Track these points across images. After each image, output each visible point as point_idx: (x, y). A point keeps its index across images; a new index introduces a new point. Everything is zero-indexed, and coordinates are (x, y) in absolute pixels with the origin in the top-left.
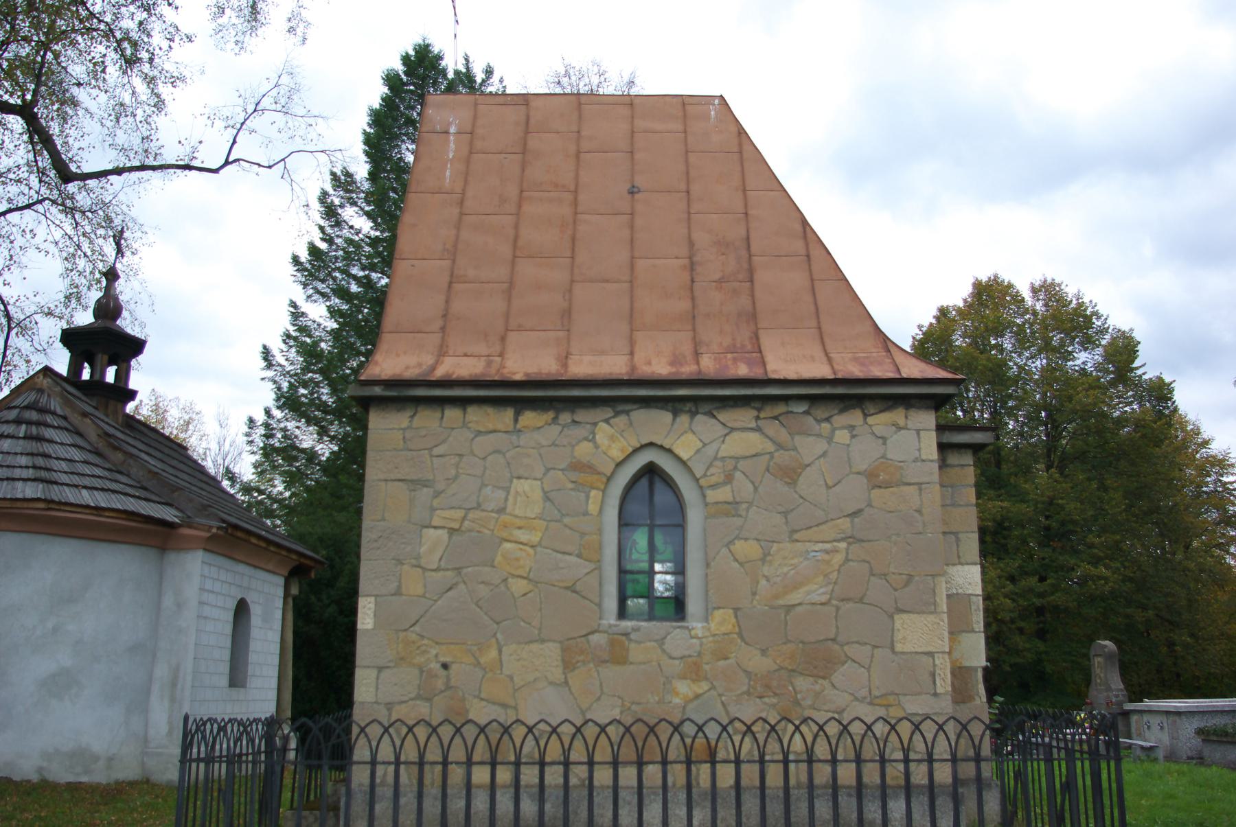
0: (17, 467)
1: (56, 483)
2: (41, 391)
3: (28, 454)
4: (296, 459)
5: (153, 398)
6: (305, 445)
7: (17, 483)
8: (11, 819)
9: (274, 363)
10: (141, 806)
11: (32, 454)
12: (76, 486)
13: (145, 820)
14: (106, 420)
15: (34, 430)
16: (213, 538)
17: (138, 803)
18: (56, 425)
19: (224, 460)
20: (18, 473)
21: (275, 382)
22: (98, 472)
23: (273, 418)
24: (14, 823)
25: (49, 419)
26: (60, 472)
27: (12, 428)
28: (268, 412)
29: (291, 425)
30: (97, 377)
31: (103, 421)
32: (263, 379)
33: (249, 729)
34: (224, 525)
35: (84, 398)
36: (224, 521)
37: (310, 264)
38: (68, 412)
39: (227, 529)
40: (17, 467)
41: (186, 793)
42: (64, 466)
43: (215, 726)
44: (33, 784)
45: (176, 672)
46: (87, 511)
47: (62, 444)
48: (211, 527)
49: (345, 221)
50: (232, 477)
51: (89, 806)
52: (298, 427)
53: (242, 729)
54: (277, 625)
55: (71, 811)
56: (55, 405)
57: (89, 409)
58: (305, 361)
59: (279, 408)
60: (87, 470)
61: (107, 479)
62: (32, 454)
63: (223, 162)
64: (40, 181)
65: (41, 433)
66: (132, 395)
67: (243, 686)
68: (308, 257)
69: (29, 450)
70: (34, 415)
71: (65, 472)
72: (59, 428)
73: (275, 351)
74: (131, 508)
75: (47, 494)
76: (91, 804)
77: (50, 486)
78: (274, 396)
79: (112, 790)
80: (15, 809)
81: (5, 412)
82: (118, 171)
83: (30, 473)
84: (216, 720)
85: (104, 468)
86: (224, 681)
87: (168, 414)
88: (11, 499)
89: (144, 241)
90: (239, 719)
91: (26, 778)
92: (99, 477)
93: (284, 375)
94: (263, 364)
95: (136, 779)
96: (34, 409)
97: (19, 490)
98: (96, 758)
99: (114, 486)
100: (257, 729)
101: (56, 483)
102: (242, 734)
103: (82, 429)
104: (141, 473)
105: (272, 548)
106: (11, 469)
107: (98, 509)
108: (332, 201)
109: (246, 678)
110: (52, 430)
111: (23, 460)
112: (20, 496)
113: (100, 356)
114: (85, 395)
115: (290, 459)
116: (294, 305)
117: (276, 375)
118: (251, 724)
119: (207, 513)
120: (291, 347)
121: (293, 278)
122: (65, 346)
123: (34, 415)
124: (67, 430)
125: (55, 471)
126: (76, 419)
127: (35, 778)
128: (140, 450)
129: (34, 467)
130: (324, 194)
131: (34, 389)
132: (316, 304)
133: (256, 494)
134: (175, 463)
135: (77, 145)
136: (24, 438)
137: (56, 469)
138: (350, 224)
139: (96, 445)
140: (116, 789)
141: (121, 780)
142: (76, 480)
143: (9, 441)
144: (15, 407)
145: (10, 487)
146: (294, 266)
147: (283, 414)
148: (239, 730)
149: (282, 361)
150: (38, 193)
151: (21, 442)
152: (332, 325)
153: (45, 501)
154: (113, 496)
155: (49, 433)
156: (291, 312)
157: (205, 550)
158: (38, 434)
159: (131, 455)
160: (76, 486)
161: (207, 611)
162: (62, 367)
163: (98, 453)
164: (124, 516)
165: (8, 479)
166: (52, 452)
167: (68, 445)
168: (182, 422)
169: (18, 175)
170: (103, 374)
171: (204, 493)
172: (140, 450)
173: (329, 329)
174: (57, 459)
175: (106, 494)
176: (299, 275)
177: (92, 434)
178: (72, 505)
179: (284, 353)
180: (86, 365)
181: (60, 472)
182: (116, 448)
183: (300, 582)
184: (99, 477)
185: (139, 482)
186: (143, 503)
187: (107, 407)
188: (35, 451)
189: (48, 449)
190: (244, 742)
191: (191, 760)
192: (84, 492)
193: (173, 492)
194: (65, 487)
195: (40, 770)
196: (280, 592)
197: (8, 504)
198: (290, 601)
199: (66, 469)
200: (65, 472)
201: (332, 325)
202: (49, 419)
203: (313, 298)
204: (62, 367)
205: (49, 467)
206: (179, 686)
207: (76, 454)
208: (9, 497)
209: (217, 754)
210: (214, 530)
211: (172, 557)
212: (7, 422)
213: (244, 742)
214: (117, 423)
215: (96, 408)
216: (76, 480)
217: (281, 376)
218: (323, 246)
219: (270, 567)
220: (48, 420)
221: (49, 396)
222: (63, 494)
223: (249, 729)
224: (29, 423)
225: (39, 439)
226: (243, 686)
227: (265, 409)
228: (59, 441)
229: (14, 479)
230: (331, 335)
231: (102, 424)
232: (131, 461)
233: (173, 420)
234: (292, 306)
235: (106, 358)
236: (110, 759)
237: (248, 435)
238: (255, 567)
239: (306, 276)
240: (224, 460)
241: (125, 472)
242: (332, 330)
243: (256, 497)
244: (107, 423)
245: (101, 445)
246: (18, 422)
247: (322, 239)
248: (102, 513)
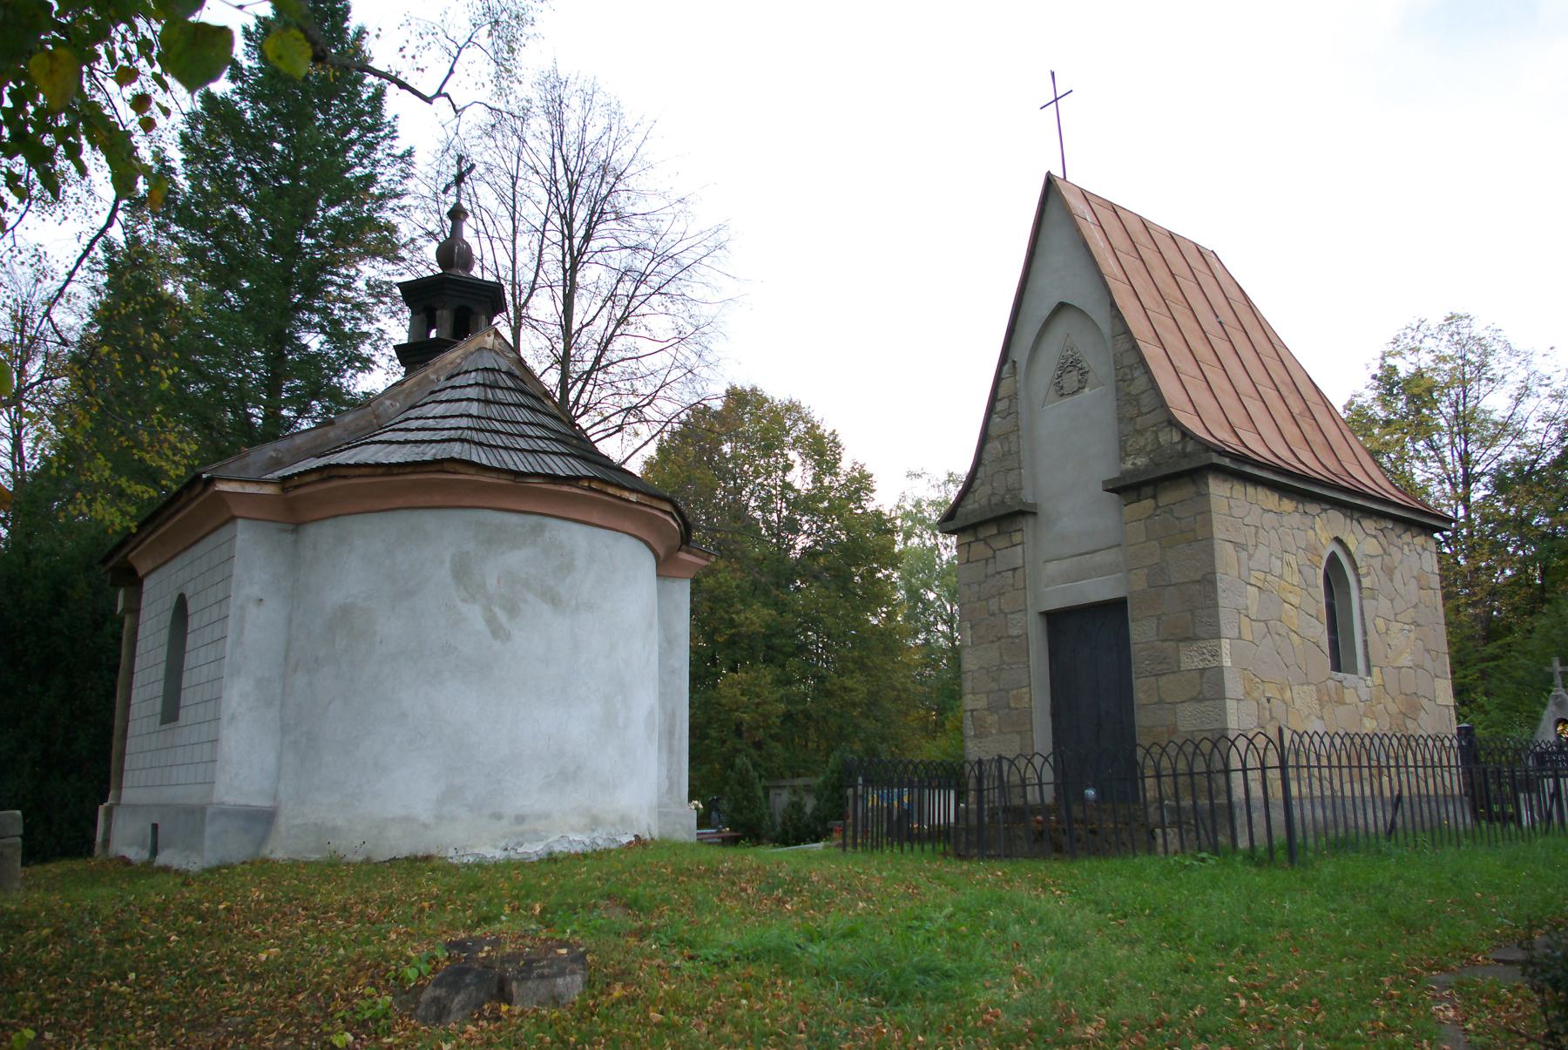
206: (677, 736)
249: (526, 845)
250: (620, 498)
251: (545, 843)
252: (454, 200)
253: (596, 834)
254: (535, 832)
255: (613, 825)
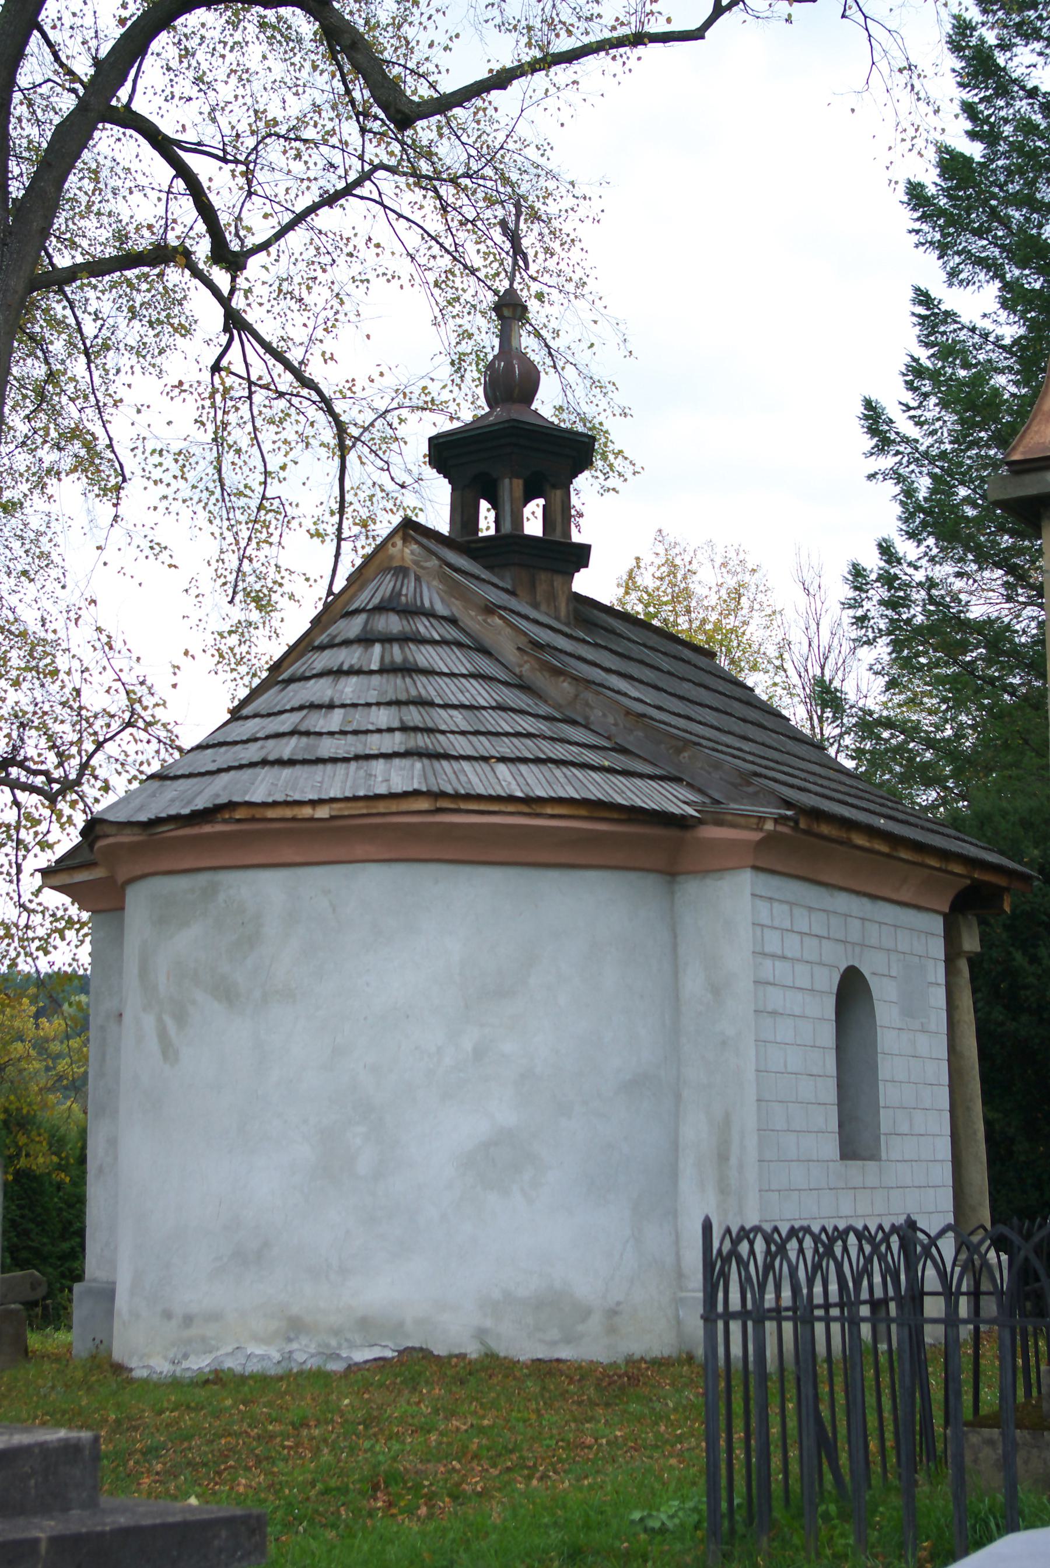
0: (372, 732)
1: (447, 757)
2: (402, 571)
3: (389, 704)
4: (964, 647)
5: (661, 549)
6: (976, 612)
7: (374, 763)
8: (429, 1432)
9: (893, 436)
10: (675, 1410)
11: (398, 703)
12: (485, 759)
13: (680, 1439)
14: (533, 614)
15: (397, 653)
16: (769, 842)
17: (671, 1404)
18: (437, 637)
19: (822, 668)
20: (328, 747)
21: (900, 479)
22: (527, 724)
23: (899, 561)
24: (433, 1437)
25: (423, 627)
26: (453, 732)
27: (357, 655)
28: (886, 550)
29: (944, 571)
30: (507, 528)
31: (526, 618)
32: (872, 476)
33: (883, 1248)
34: (789, 813)
35: (485, 575)
36: (788, 804)
37: (950, 197)
38: (457, 608)
39: (797, 822)
40: (372, 732)
41: (722, 1384)
42: (459, 719)
43: (808, 1242)
44: (470, 1362)
45: (724, 1128)
46: (510, 808)
47: (452, 675)
48: (762, 819)
49: (1014, 81)
50: (832, 700)
51: (574, 1407)
52: (959, 575)
53: (868, 1249)
54: (939, 1021)
55: (540, 1415)
56: (432, 597)
57: (495, 596)
58: (962, 421)
59: (911, 535)
60: (504, 723)
61: (545, 738)
62: (398, 703)
63: (708, 10)
64: (363, 131)
65: (411, 659)
66: (580, 556)
67: (873, 1155)
68: (938, 181)
69: (390, 696)
70: (392, 624)
71: (463, 733)
72: (444, 642)
73: (893, 412)
74: (595, 793)
75: (432, 780)
76: (579, 1403)
77: (436, 764)
78: (898, 510)
79: (620, 1377)
80: (436, 1411)
81: (342, 624)
82: (501, 80)
83: (396, 742)
84: (807, 1230)
85: (536, 716)
86: (831, 1147)
87: (695, 578)
88: (366, 798)
89: (582, 212)
90: (860, 1227)
91: (457, 1352)
92: (529, 735)
93: (917, 460)
94: (869, 442)
95: (666, 1354)
96: (393, 610)
97: (380, 779)
98: (585, 1313)
99: (559, 751)
100: (801, 1251)
101: (447, 757)
102: (869, 1260)
103: (488, 641)
104: (611, 720)
105: (904, 854)
106: (362, 737)
107: (531, 802)
108: (981, 39)
109: (878, 1139)
110: (430, 648)
111: (383, 717)
112: (382, 790)
113: (507, 481)
114: (488, 567)
115: (954, 650)
116: (923, 298)
117: (900, 463)
118: (832, 1240)
119: (751, 789)
120: (926, 395)
121: (914, 238)
122: (439, 472)
123: (392, 624)
124: (459, 645)
125: (443, 732)
126: (472, 619)
127: (473, 1350)
128: (608, 671)
129: (404, 729)
130: (963, 27)
131: (389, 569)
132: (970, 288)
133: (886, 735)
134: (686, 689)
135: (424, 38)
136: (381, 671)
137: (443, 727)
138: (1030, 85)
139: (517, 670)
140: (626, 1374)
141: (637, 1357)
142: (484, 746)
143: (354, 680)
144: (357, 612)
145: (362, 773)
146: (914, 209)
147: (922, 549)
148: (861, 1249)
149: (912, 431)
150: (361, 158)
151: (376, 680)
152: (1010, 330)
153: (429, 794)
154: (557, 772)
155: (425, 656)
156: (919, 316)
157: (755, 868)
158: (405, 660)
159: (589, 683)
160: (485, 759)
161: (776, 998)
162: (438, 517)
163: (524, 687)
164: (583, 812)
165: (357, 758)
166: (433, 693)
167: (463, 676)
168: (723, 593)
169: (324, 126)
170: (518, 521)
171: (747, 746)
172: (608, 671)
173: (1007, 341)
174: (446, 706)
175: (543, 768)
176: (925, 227)
177: (507, 647)
178: (479, 798)
179: (912, 413)
180: (484, 505)
181: (453, 732)
182: (557, 672)
183: (983, 922)
184: (529, 735)
185: (608, 738)
186: (619, 781)
187: (533, 587)
188: (403, 697)
189: (426, 688)
190: (877, 1279)
191: (728, 1316)
192: (502, 769)
193: (679, 751)
194: (465, 764)
195: (481, 1334)
196: (937, 946)
197: (361, 808)
198: (964, 966)
199: (464, 726)
200: (463, 733)
201: (1010, 330)
202: (423, 627)
203: (962, 276)
204: (438, 517)
205: (430, 725)
206: (733, 1161)
207: (478, 693)
208: (361, 793)
209: (818, 1299)
210: (769, 826)
211: (691, 889)
212: (347, 643)
213: (877, 1279)
214: (557, 618)
215: (512, 593)
216: (484, 746)
217: (909, 463)
218: (975, 151)
219: (905, 896)
220: (422, 630)
221: (418, 579)
222: (463, 779)
223: (883, 1248)
224: (387, 640)
225: (409, 670)
226: (873, 1155)
227: (880, 546)
228: (446, 670)
229: (368, 757)
230: (1013, 354)
231: (524, 625)
232: (589, 696)
233: (705, 592)
234: (920, 303)
235: (518, 484)
236: (613, 1313)
237: (855, 604)
238: (874, 897)
239: (942, 229)
240: (822, 668)
241: (580, 719)
242: (1016, 342)
243: (887, 741)
244: (536, 622)
245: (527, 669)
246: (366, 640)
247: (972, 135)
248: (538, 810)
249: (192, 1358)
250: (294, 819)
251: (213, 1356)
252: (506, 284)
253: (295, 1346)
254: (204, 1339)
255: (337, 1332)
